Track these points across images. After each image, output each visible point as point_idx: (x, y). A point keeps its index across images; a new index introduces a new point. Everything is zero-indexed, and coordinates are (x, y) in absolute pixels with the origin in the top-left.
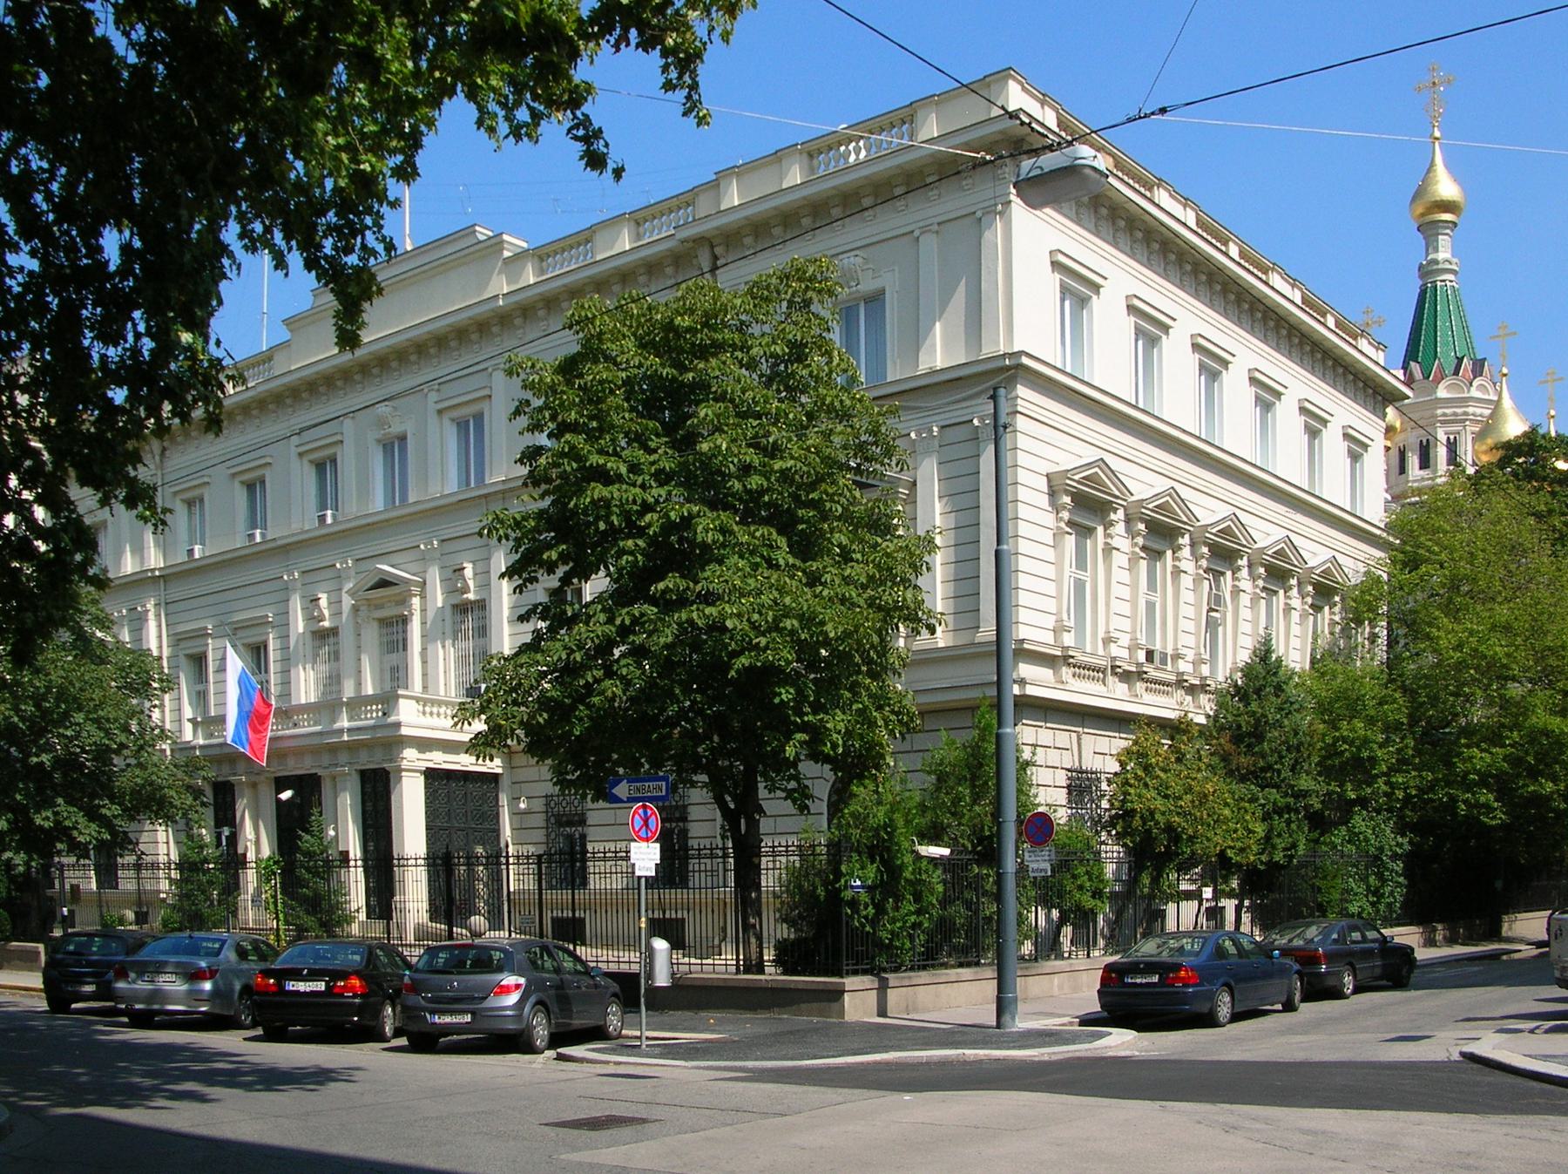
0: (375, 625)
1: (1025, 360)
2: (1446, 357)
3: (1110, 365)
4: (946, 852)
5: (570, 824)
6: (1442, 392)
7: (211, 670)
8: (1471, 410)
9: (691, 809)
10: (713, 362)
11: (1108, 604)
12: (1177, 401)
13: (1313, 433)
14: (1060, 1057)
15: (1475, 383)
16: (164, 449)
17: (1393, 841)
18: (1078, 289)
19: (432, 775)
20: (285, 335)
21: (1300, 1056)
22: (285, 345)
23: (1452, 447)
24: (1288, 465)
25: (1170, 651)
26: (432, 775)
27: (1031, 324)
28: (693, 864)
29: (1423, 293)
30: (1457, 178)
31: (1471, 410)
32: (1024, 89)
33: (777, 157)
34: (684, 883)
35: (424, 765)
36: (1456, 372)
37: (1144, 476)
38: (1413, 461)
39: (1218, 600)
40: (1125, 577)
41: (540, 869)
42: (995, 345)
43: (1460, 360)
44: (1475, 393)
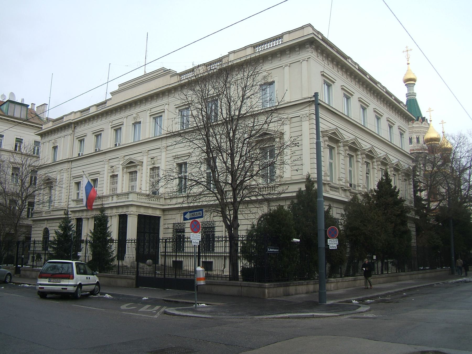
0: (128, 174)
4: (299, 240)
5: (180, 232)
7: (284, 283)
9: (216, 228)
10: (239, 239)
11: (339, 170)
12: (355, 114)
13: (390, 127)
15: (423, 123)
16: (75, 127)
20: (111, 97)
22: (110, 99)
23: (418, 139)
24: (385, 134)
25: (356, 184)
28: (216, 244)
33: (245, 48)
34: (120, 216)
37: (348, 134)
39: (369, 170)
40: (343, 162)
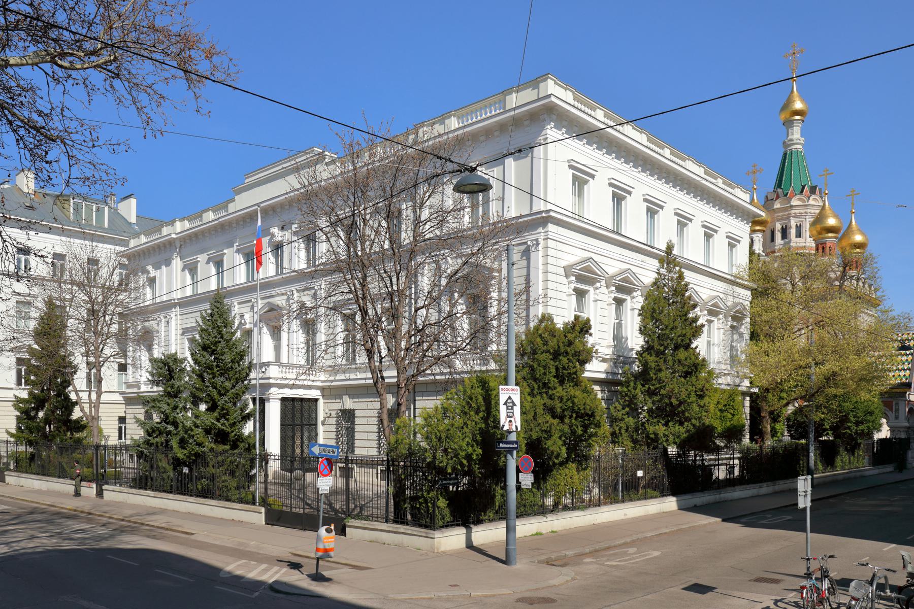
1: (552, 214)
2: (796, 184)
3: (597, 208)
6: (794, 202)
8: (809, 211)
14: (831, 478)
17: (534, 437)
18: (581, 179)
19: (284, 400)
21: (122, 500)
26: (284, 400)
27: (557, 194)
29: (785, 154)
30: (803, 99)
31: (809, 211)
32: (556, 83)
35: (280, 396)
36: (802, 191)
38: (778, 235)
41: (466, 373)
42: (539, 206)
43: (803, 187)
44: (811, 202)
